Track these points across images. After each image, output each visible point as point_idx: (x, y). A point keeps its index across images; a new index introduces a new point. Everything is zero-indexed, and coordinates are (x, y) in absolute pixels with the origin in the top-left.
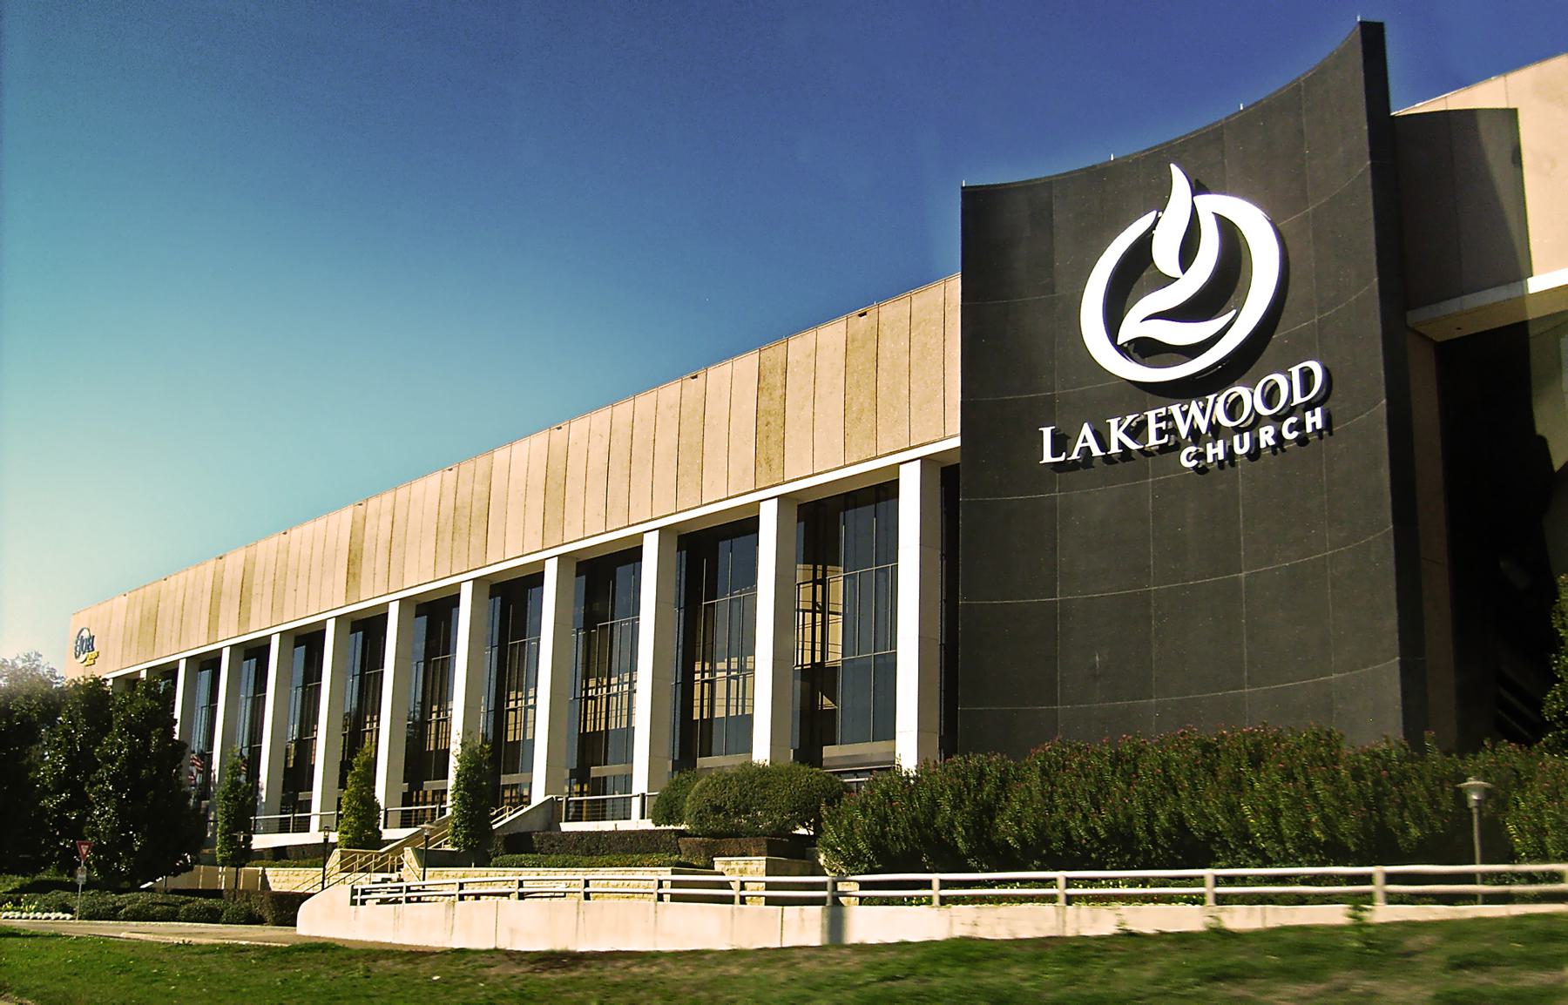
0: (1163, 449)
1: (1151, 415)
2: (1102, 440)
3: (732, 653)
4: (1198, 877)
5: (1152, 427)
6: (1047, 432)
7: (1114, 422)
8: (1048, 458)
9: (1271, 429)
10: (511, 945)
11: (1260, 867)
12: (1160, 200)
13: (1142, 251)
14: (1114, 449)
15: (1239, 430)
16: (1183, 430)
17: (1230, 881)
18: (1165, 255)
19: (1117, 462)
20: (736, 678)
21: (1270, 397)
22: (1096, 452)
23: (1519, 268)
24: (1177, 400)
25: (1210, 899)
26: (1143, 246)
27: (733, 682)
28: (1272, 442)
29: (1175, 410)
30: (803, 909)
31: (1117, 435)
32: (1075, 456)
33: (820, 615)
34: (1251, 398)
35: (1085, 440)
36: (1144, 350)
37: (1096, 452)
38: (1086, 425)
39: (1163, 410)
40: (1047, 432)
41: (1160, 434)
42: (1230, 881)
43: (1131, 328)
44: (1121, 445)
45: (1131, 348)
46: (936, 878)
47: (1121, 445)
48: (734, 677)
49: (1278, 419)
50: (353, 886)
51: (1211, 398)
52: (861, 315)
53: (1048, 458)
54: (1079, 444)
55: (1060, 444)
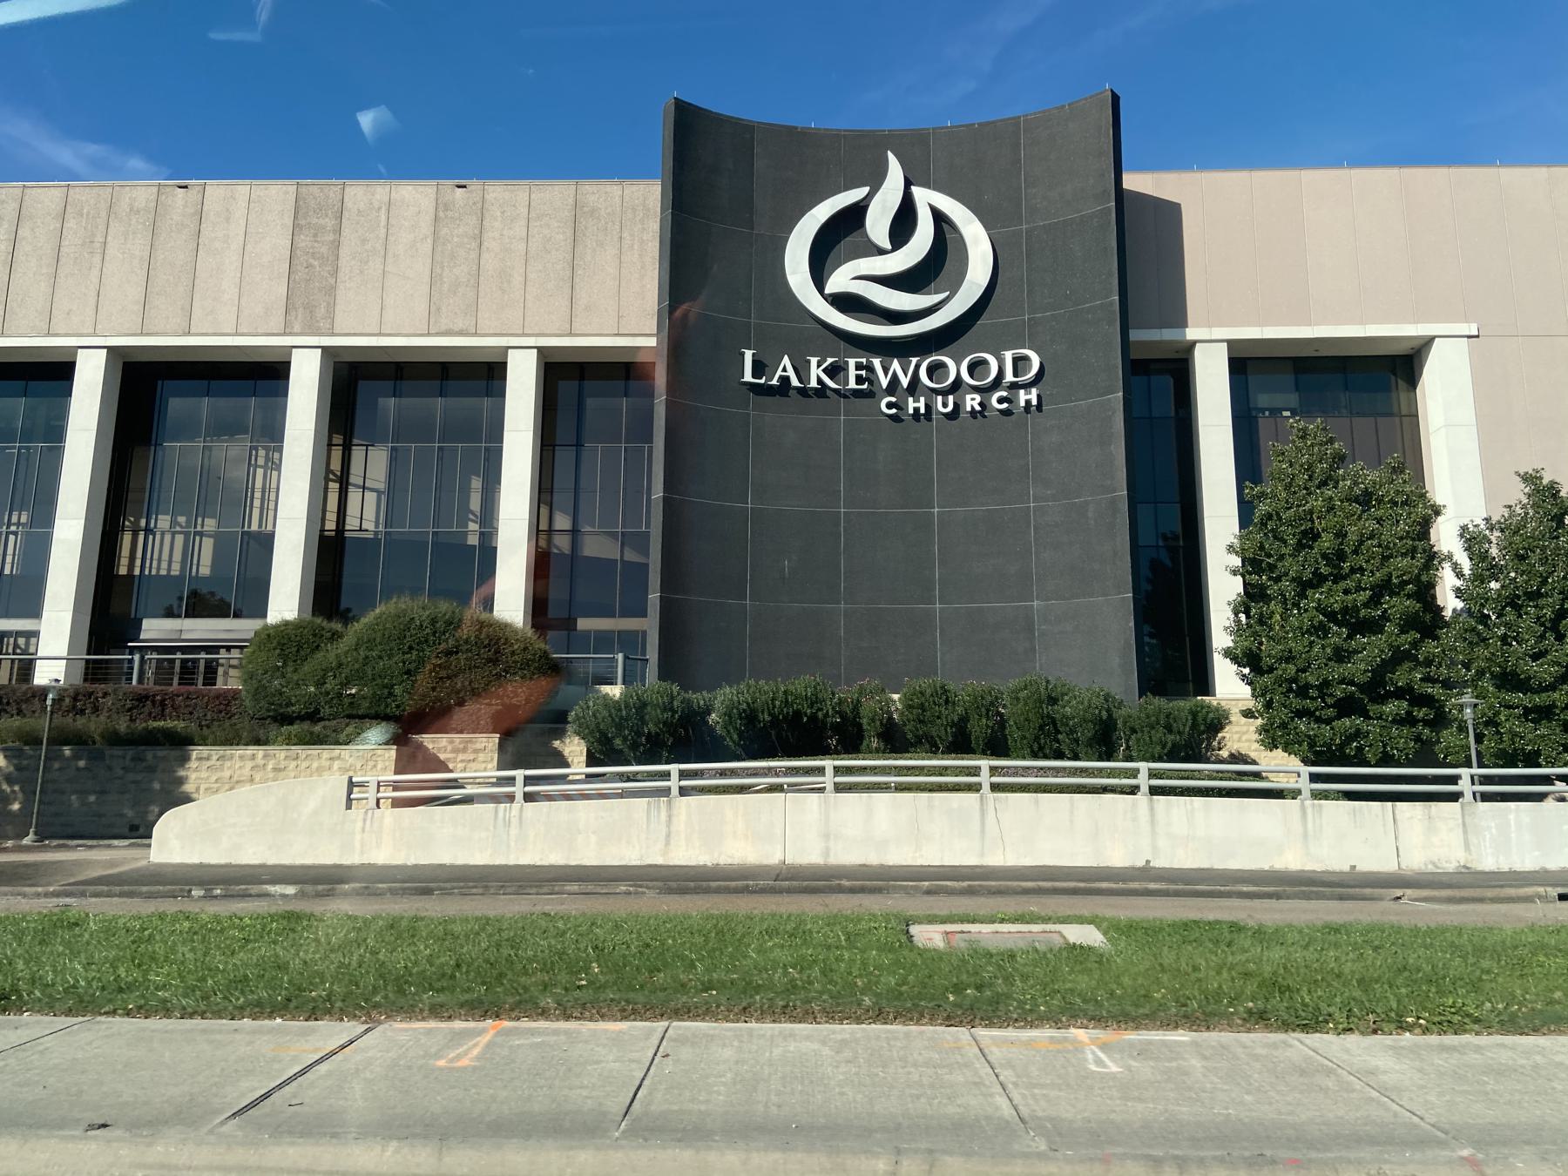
0: (856, 393)
1: (852, 362)
2: (802, 372)
3: (15, 506)
4: (972, 767)
5: (852, 373)
6: (749, 355)
7: (814, 361)
8: (748, 377)
9: (978, 398)
10: (665, 854)
11: (1502, 767)
12: (876, 179)
13: (853, 217)
14: (814, 383)
15: (976, 389)
16: (884, 382)
17: (849, 771)
18: (878, 225)
19: (810, 397)
20: (15, 533)
21: (976, 367)
22: (795, 382)
23: (1183, 324)
24: (861, 352)
25: (986, 787)
26: (853, 217)
27: (12, 537)
28: (978, 408)
29: (877, 362)
30: (1320, 806)
31: (816, 372)
32: (774, 382)
33: (337, 485)
34: (956, 368)
35: (784, 370)
36: (847, 303)
37: (795, 382)
38: (786, 356)
39: (864, 360)
40: (749, 355)
41: (859, 380)
42: (849, 771)
43: (841, 280)
44: (820, 381)
45: (830, 299)
46: (674, 768)
47: (820, 381)
48: (13, 533)
49: (984, 391)
50: (351, 778)
51: (914, 360)
52: (459, 187)
53: (748, 377)
54: (779, 373)
55: (759, 369)
